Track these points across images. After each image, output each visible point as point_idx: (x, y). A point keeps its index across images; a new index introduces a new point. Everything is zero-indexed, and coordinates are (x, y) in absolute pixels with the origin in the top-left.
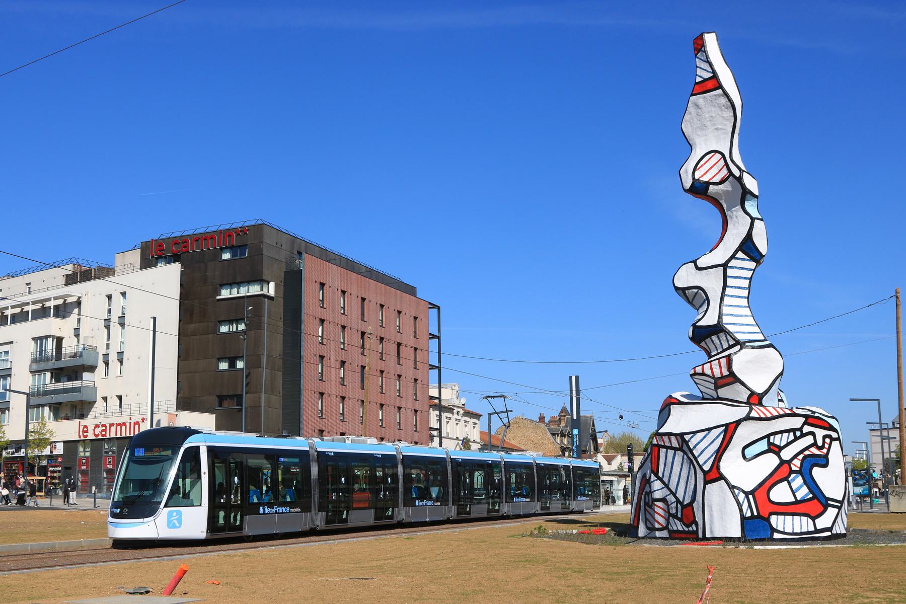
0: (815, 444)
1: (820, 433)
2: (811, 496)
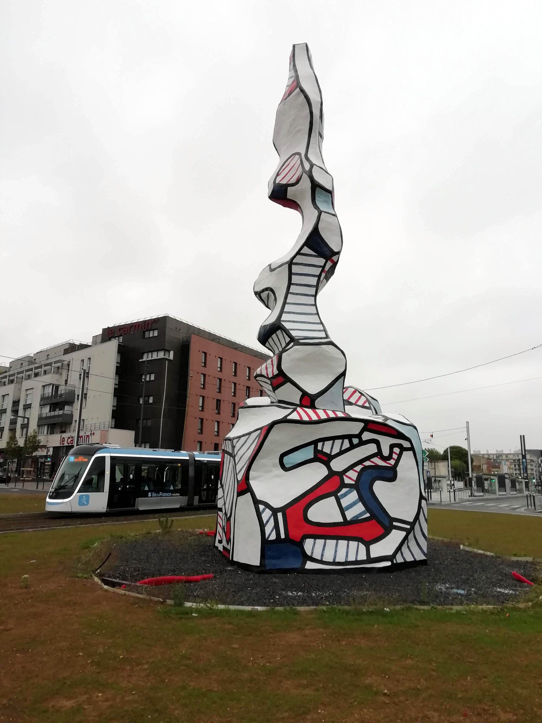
0: (379, 453)
1: (386, 442)
2: (368, 515)
